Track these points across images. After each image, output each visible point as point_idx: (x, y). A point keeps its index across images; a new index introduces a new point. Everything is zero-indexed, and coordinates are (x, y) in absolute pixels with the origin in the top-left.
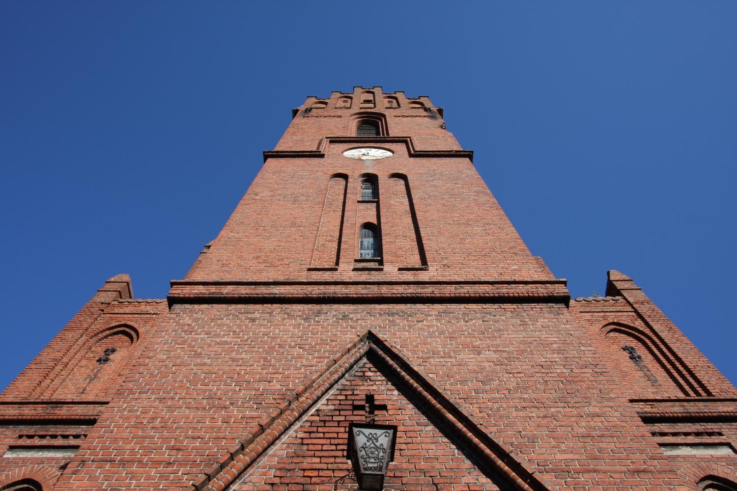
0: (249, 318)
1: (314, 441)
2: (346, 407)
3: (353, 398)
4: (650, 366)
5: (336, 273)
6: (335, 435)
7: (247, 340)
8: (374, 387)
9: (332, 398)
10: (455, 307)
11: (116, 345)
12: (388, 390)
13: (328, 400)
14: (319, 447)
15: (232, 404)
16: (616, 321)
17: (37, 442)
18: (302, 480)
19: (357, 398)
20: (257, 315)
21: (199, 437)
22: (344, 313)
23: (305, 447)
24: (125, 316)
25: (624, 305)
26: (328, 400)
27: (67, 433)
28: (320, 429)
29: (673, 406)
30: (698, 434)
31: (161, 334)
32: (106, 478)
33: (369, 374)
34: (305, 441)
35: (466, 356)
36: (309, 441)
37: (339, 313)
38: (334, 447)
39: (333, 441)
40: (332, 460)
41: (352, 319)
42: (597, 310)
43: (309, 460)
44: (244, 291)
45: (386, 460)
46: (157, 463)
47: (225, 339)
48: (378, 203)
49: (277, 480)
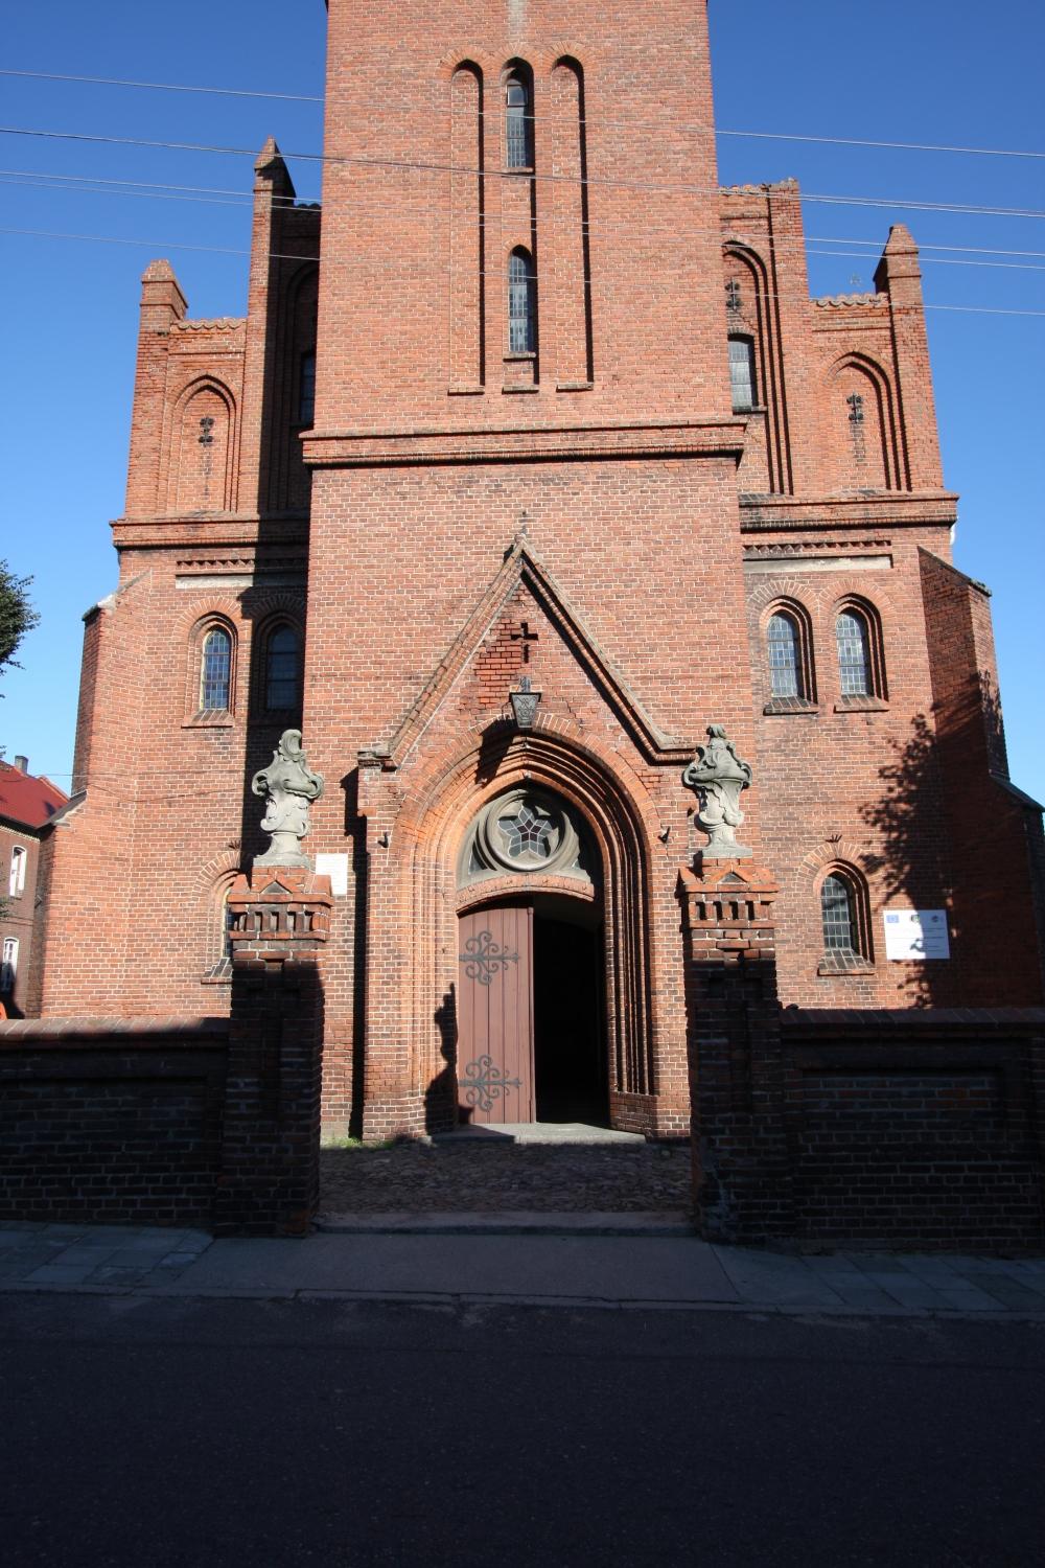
4: (868, 437)
6: (499, 666)
9: (494, 627)
10: (615, 467)
15: (409, 615)
16: (856, 350)
17: (196, 569)
18: (477, 705)
20: (405, 488)
24: (199, 358)
29: (855, 510)
30: (867, 544)
32: (337, 691)
35: (615, 548)
37: (492, 481)
40: (498, 689)
42: (839, 327)
44: (384, 450)
46: (368, 678)
48: (536, 361)
49: (463, 707)
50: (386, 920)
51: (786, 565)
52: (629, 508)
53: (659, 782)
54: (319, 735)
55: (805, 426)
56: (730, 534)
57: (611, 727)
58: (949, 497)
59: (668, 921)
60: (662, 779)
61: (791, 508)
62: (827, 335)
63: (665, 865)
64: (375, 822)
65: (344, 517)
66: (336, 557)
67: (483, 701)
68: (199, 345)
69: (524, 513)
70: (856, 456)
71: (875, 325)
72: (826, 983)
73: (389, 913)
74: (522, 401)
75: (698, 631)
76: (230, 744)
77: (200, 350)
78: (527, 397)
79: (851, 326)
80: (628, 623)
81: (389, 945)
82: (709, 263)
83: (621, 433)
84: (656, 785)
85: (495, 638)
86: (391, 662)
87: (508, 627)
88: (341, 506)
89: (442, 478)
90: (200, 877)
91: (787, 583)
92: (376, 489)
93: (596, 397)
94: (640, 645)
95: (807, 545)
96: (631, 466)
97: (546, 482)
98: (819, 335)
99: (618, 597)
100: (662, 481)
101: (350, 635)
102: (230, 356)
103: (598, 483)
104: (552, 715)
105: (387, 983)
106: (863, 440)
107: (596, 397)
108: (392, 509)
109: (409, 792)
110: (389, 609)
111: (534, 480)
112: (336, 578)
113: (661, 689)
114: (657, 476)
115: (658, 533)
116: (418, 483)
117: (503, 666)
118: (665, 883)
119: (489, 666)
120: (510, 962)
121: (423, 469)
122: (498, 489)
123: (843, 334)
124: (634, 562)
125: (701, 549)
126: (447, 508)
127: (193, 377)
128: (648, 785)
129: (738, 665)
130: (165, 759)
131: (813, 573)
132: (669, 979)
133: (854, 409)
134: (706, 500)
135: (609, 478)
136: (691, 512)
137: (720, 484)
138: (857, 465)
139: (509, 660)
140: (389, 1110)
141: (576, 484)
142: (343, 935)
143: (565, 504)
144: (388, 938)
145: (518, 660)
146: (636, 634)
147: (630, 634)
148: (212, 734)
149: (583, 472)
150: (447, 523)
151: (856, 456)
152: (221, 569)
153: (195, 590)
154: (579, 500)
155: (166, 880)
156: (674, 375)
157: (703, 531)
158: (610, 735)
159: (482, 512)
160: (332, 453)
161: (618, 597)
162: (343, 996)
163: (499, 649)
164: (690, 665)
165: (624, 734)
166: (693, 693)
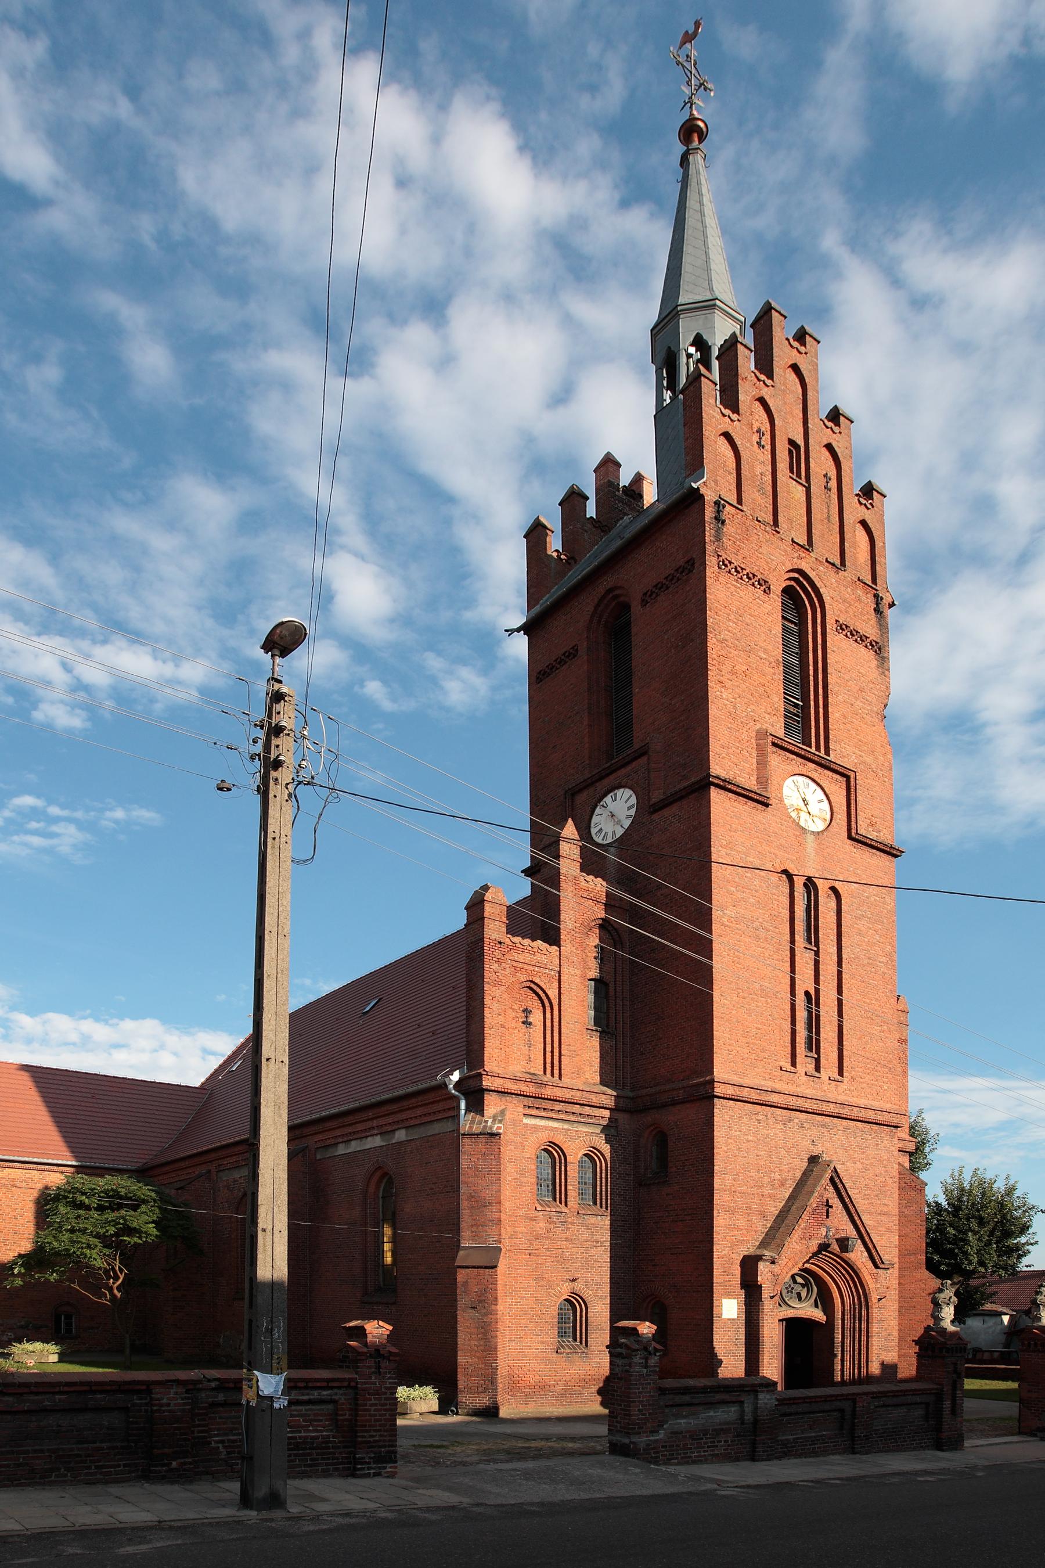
20: (760, 1117)
35: (850, 1165)
44: (754, 1096)
64: (766, 1287)
74: (813, 1081)
77: (527, 962)
78: (815, 1079)
82: (892, 1028)
90: (551, 1296)
97: (823, 1126)
122: (802, 1126)
130: (525, 1227)
136: (880, 1152)
150: (779, 1140)
155: (531, 1297)
160: (729, 1092)
165: (866, 1254)
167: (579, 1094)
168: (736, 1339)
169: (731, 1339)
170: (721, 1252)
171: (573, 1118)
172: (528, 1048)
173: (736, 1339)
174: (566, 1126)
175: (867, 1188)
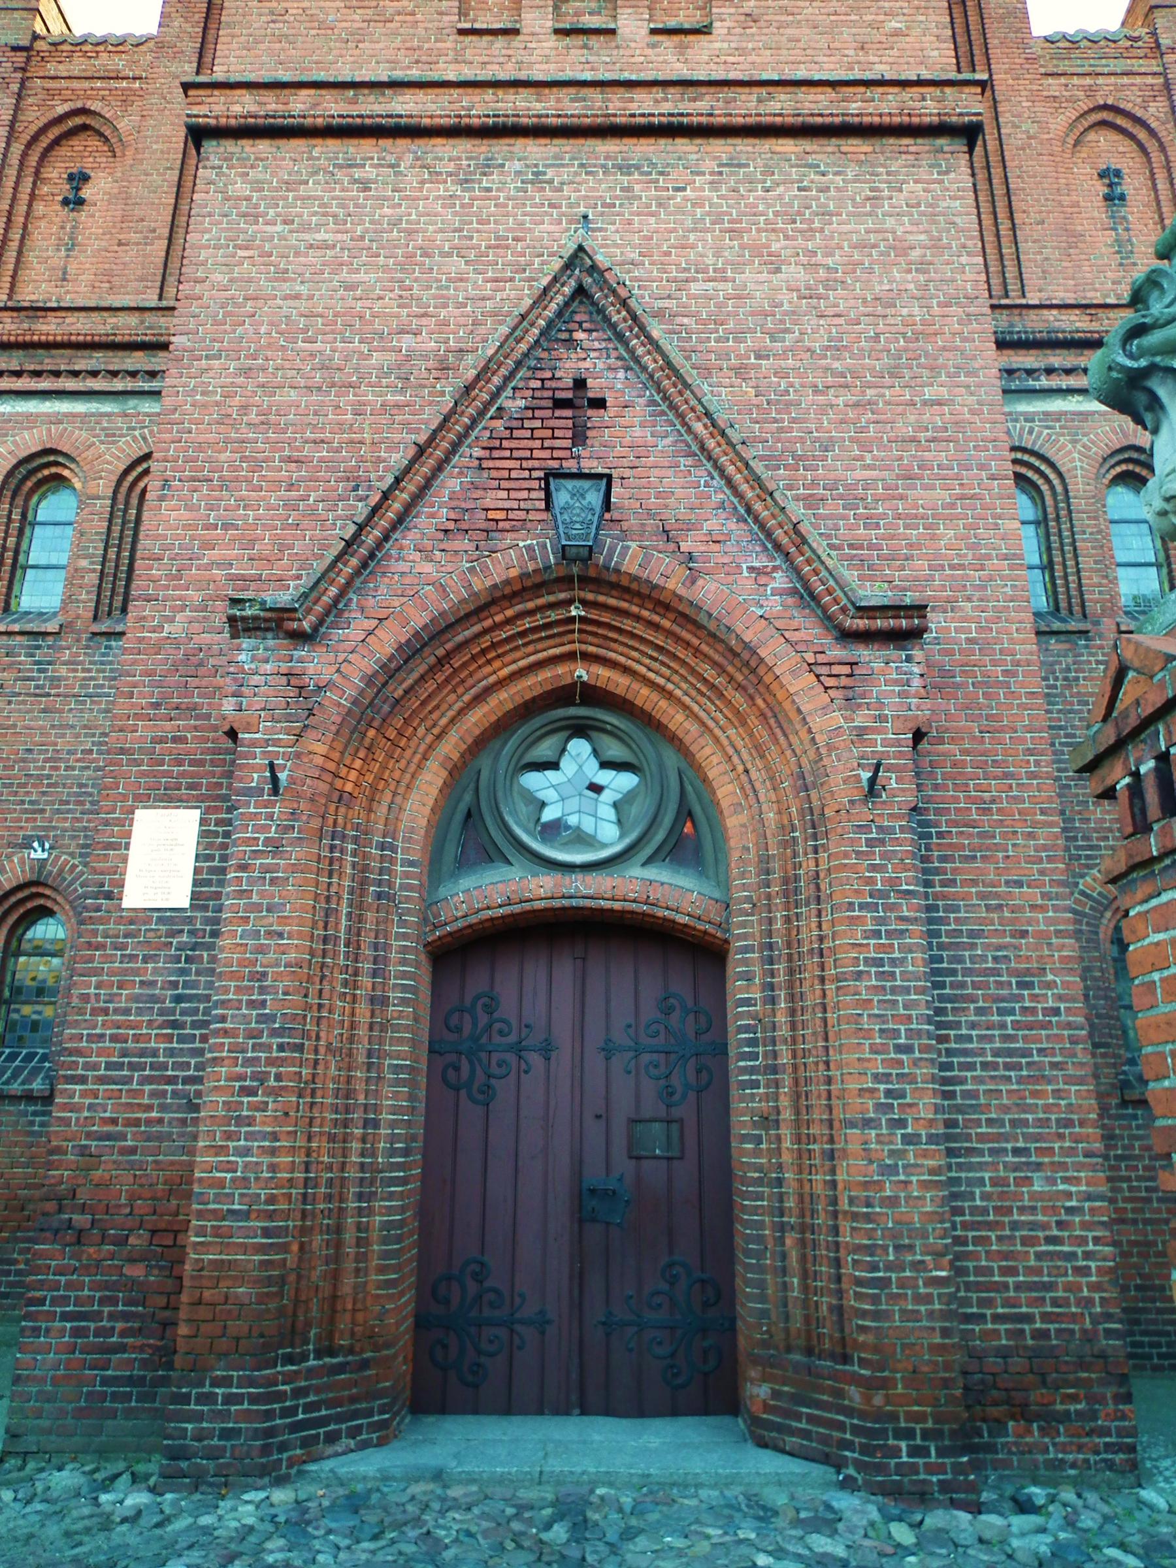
0: (356, 181)
1: (499, 464)
2: (544, 403)
3: (554, 384)
4: (1136, 226)
5: (517, 42)
6: (527, 454)
7: (362, 238)
8: (587, 364)
10: (750, 149)
11: (88, 164)
12: (610, 368)
13: (514, 389)
14: (505, 474)
16: (1110, 102)
18: (484, 525)
19: (560, 385)
20: (370, 172)
21: (323, 441)
22: (536, 166)
23: (485, 474)
24: (75, 84)
25: (1146, 57)
26: (514, 389)
27: (77, 368)
28: (505, 444)
31: (202, 223)
33: (580, 335)
34: (485, 464)
35: (752, 278)
36: (490, 464)
37: (527, 166)
38: (526, 474)
39: (525, 464)
40: (525, 494)
41: (551, 182)
42: (1080, 70)
43: (491, 494)
44: (334, 107)
45: (598, 510)
47: (322, 236)
49: (451, 525)
50: (261, 950)
51: (1019, 400)
52: (776, 214)
53: (851, 675)
54: (167, 588)
55: (1038, 201)
56: (964, 259)
57: (751, 569)
58: (520, 1163)
59: (879, 962)
60: (857, 671)
61: (1024, 312)
62: (1063, 80)
63: (870, 843)
64: (253, 743)
65: (253, 217)
66: (231, 280)
67: (492, 514)
68: (78, 65)
69: (585, 217)
70: (1118, 252)
71: (1136, 69)
72: (1135, 1117)
73: (269, 934)
74: (585, 47)
75: (912, 418)
76: (49, 663)
79: (1099, 70)
80: (778, 402)
81: (263, 1004)
83: (764, 91)
84: (844, 681)
85: (522, 403)
86: (321, 460)
87: (548, 384)
88: (249, 199)
89: (436, 158)
91: (1022, 429)
92: (316, 173)
93: (718, 45)
94: (802, 440)
95: (1049, 371)
96: (779, 149)
98: (1050, 80)
99: (758, 357)
100: (837, 174)
101: (244, 408)
102: (124, 84)
103: (721, 173)
104: (633, 545)
105: (251, 1092)
106: (1127, 229)
107: (718, 45)
108: (343, 206)
109: (329, 685)
110: (323, 367)
111: (603, 166)
112: (226, 314)
113: (845, 518)
114: (827, 165)
115: (832, 255)
116: (391, 166)
117: (536, 454)
118: (871, 881)
119: (507, 454)
120: (535, 1058)
121: (402, 143)
123: (1088, 81)
124: (787, 299)
125: (911, 282)
126: (444, 206)
127: (61, 109)
128: (830, 682)
129: (992, 478)
131: (1065, 413)
132: (889, 1093)
133: (1110, 185)
134: (919, 205)
135: (740, 166)
136: (890, 222)
137: (942, 181)
138: (1121, 265)
139: (547, 443)
140: (229, 1399)
141: (678, 175)
142: (175, 985)
143: (660, 205)
144: (263, 990)
145: (567, 443)
146: (794, 421)
147: (783, 421)
148: (22, 647)
149: (694, 157)
151: (1118, 252)
152: (71, 384)
153: (18, 414)
154: (686, 199)
156: (853, 17)
157: (915, 254)
158: (750, 585)
159: (507, 215)
161: (758, 357)
162: (160, 1121)
163: (527, 424)
164: (898, 477)
166: (906, 527)
167: (133, 320)
168: (178, 999)
169: (154, 999)
170: (160, 628)
171: (118, 385)
172: (63, 253)
173: (178, 999)
174: (107, 407)
175: (836, 349)
